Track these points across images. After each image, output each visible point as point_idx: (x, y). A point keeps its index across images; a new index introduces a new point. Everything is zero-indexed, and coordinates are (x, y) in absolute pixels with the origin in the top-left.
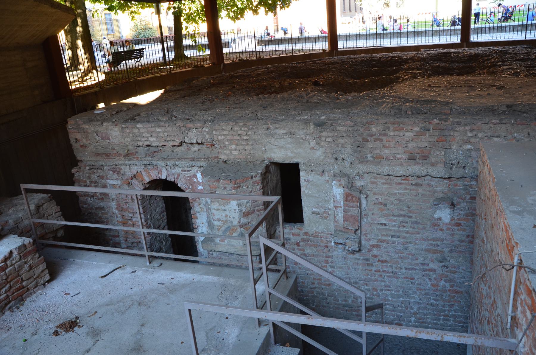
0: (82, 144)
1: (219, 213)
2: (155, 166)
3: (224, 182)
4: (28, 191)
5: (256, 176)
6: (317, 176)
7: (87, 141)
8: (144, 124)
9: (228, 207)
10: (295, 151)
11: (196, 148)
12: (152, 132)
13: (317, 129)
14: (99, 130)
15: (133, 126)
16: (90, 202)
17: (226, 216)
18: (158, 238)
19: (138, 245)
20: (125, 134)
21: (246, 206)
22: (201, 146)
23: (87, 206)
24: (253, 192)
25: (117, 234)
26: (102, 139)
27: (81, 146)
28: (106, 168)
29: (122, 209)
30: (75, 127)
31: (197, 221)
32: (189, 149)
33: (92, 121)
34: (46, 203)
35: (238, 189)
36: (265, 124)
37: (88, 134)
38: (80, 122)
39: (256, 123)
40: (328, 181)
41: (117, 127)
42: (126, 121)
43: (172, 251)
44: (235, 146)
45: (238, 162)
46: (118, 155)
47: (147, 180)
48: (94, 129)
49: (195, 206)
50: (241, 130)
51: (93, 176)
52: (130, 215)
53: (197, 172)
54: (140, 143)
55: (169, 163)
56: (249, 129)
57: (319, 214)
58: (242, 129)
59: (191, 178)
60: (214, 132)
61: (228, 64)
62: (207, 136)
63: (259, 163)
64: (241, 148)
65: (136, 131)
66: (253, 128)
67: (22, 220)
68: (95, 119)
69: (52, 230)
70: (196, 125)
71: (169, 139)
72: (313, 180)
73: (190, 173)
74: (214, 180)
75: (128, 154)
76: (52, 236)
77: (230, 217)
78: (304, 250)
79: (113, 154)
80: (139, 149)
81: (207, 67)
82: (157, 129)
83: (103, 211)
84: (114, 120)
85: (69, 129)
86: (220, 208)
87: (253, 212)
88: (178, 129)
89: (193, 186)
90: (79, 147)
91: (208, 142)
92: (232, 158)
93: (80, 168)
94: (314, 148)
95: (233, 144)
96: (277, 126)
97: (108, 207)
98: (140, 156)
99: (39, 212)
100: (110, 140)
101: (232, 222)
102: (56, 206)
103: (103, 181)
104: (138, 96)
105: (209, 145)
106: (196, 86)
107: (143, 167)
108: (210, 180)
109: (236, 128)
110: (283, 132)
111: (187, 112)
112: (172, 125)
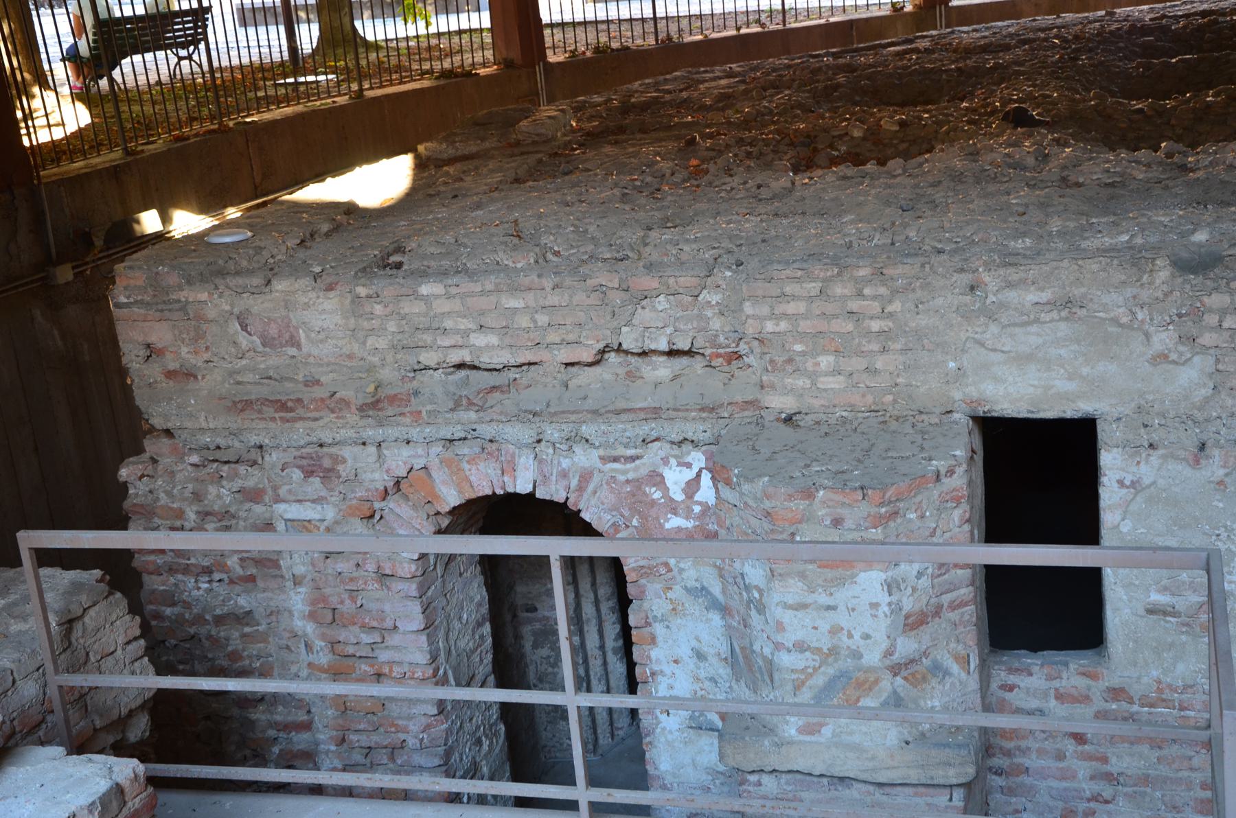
0: (173, 366)
1: (806, 618)
2: (487, 445)
3: (831, 495)
4: (46, 557)
5: (951, 472)
6: (1174, 466)
7: (196, 353)
8: (450, 282)
9: (842, 596)
10: (1085, 371)
11: (662, 369)
12: (482, 313)
13: (1189, 282)
14: (255, 310)
15: (404, 291)
16: (195, 593)
17: (835, 630)
18: (467, 726)
19: (392, 758)
20: (366, 324)
21: (914, 589)
22: (685, 360)
23: (177, 610)
24: (938, 532)
25: (302, 717)
26: (264, 345)
27: (170, 374)
28: (273, 458)
29: (335, 617)
30: (147, 298)
31: (654, 653)
32: (632, 376)
33: (222, 273)
34: (94, 605)
35: (892, 524)
36: (962, 270)
37: (204, 327)
38: (173, 279)
39: (923, 266)
40: (1221, 483)
41: (332, 294)
42: (365, 272)
43: (508, 774)
44: (831, 358)
45: (844, 421)
46: (333, 403)
47: (452, 498)
48: (232, 305)
49: (649, 594)
50: (860, 294)
51: (213, 490)
52: (366, 638)
53: (665, 461)
54: (428, 358)
55: (552, 432)
56: (895, 292)
57: (1175, 614)
58: (867, 291)
59: (639, 488)
60: (748, 308)
61: (559, 63)
62: (716, 324)
63: (935, 420)
64: (858, 363)
65: (414, 308)
66: (908, 288)
67: (14, 682)
68: (231, 266)
69: (115, 715)
70: (671, 281)
71: (553, 337)
72: (1154, 483)
73: (636, 469)
74: (791, 490)
75: (378, 401)
76: (111, 739)
77: (850, 636)
78: (1104, 760)
79: (314, 400)
80: (425, 379)
81: (487, 77)
82: (504, 301)
83: (247, 630)
84: (318, 269)
85: (117, 305)
86: (810, 599)
87: (937, 612)
88: (594, 299)
89: (644, 517)
90: (161, 377)
91: (720, 346)
92: (817, 403)
93: (154, 461)
94: (1166, 357)
95: (825, 351)
96: (1015, 277)
97: (274, 613)
98: (429, 407)
99: (70, 643)
100: (298, 346)
101: (857, 655)
102: (128, 617)
103: (258, 509)
104: (329, 180)
105: (718, 356)
106: (534, 143)
107: (437, 449)
108: (771, 490)
109: (839, 290)
110: (1036, 299)
111: (598, 234)
112: (568, 282)
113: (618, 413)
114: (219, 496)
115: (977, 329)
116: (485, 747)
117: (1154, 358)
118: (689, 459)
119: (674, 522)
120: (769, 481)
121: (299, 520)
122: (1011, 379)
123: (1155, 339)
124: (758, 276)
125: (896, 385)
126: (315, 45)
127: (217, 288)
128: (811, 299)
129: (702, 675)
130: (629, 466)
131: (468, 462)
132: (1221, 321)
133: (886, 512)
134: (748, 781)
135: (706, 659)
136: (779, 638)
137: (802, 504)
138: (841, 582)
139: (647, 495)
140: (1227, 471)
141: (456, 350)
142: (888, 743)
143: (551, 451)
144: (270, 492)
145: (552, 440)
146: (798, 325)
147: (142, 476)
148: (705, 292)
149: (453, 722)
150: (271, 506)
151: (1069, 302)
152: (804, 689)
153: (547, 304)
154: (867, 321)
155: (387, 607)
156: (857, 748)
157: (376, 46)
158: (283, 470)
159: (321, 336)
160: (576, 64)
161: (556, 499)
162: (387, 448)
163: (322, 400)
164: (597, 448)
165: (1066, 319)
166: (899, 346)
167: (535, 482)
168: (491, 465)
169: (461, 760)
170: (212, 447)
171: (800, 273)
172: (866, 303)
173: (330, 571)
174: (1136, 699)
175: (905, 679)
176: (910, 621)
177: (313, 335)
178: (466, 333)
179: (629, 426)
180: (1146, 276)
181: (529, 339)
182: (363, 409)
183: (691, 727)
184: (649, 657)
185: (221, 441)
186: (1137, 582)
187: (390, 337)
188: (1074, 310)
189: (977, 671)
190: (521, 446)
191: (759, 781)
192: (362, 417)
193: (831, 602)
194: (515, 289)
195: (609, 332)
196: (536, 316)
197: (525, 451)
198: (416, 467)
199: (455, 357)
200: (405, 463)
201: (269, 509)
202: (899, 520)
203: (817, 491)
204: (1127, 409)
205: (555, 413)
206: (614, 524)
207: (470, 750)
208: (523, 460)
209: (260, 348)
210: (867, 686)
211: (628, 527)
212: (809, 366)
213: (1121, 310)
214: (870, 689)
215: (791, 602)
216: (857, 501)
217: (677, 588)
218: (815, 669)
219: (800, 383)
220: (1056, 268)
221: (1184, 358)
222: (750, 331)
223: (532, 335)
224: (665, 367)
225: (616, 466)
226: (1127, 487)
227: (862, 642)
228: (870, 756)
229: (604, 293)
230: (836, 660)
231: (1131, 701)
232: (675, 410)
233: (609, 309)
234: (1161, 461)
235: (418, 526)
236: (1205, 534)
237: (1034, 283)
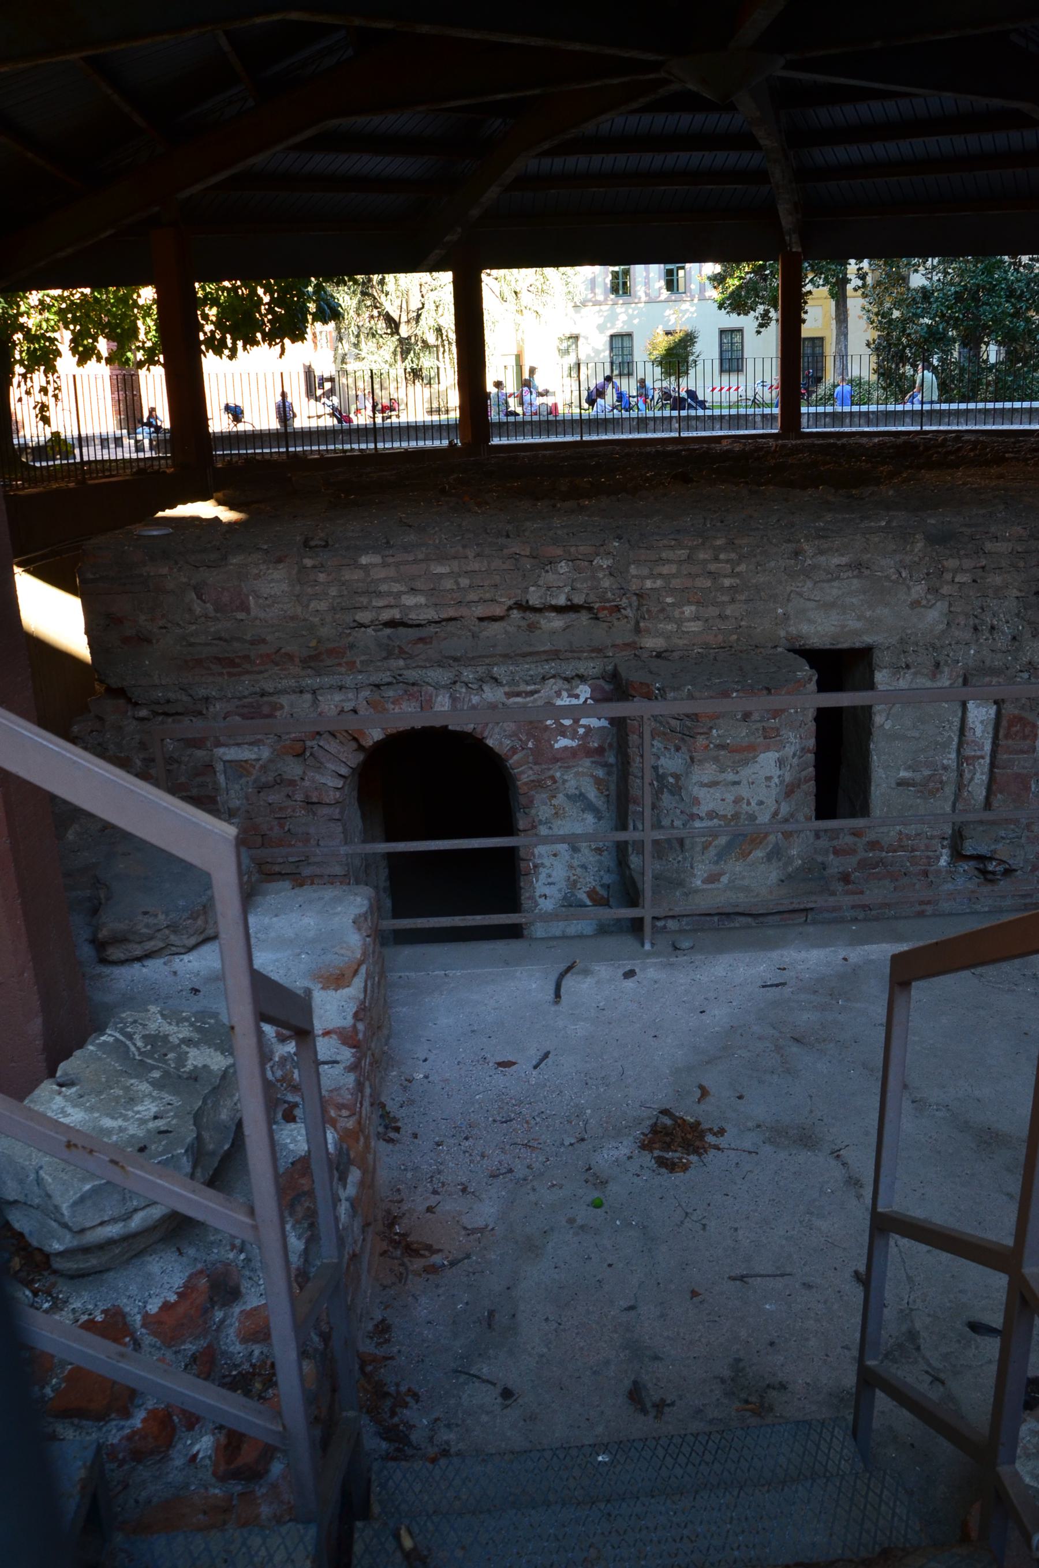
1: (717, 793)
8: (387, 553)
9: (746, 773)
11: (556, 622)
32: (532, 627)
36: (789, 541)
39: (762, 537)
41: (281, 566)
50: (716, 559)
54: (364, 617)
55: (468, 675)
56: (742, 558)
58: (722, 556)
60: (633, 570)
62: (606, 583)
64: (712, 611)
65: (358, 575)
70: (573, 549)
71: (473, 596)
73: (535, 700)
77: (749, 804)
86: (722, 777)
91: (609, 601)
92: (681, 642)
96: (826, 546)
98: (363, 658)
100: (246, 609)
101: (752, 817)
104: (189, 504)
107: (366, 693)
109: (701, 556)
113: (524, 655)
117: (912, 604)
118: (577, 691)
119: (563, 742)
121: (236, 761)
122: (820, 620)
125: (740, 627)
128: (680, 562)
129: (576, 863)
130: (528, 699)
131: (393, 703)
132: (953, 577)
134: (656, 926)
135: (579, 851)
136: (695, 810)
138: (746, 762)
141: (388, 610)
145: (466, 680)
146: (670, 583)
147: (92, 731)
150: (212, 750)
152: (711, 848)
153: (469, 569)
155: (312, 830)
165: (857, 577)
166: (744, 598)
168: (412, 705)
171: (673, 543)
172: (720, 565)
173: (262, 803)
177: (261, 601)
178: (398, 595)
179: (533, 666)
181: (452, 599)
183: (564, 906)
184: (533, 854)
185: (171, 695)
187: (331, 600)
190: (437, 687)
191: (665, 925)
192: (304, 668)
193: (736, 778)
194: (442, 558)
196: (460, 580)
197: (442, 691)
199: (386, 616)
200: (336, 706)
201: (209, 752)
204: (894, 640)
206: (512, 747)
208: (440, 698)
210: (758, 841)
211: (523, 749)
212: (677, 614)
213: (892, 570)
214: (761, 843)
215: (706, 781)
219: (669, 627)
225: (519, 700)
227: (757, 808)
231: (882, 849)
235: (344, 760)
236: (937, 727)
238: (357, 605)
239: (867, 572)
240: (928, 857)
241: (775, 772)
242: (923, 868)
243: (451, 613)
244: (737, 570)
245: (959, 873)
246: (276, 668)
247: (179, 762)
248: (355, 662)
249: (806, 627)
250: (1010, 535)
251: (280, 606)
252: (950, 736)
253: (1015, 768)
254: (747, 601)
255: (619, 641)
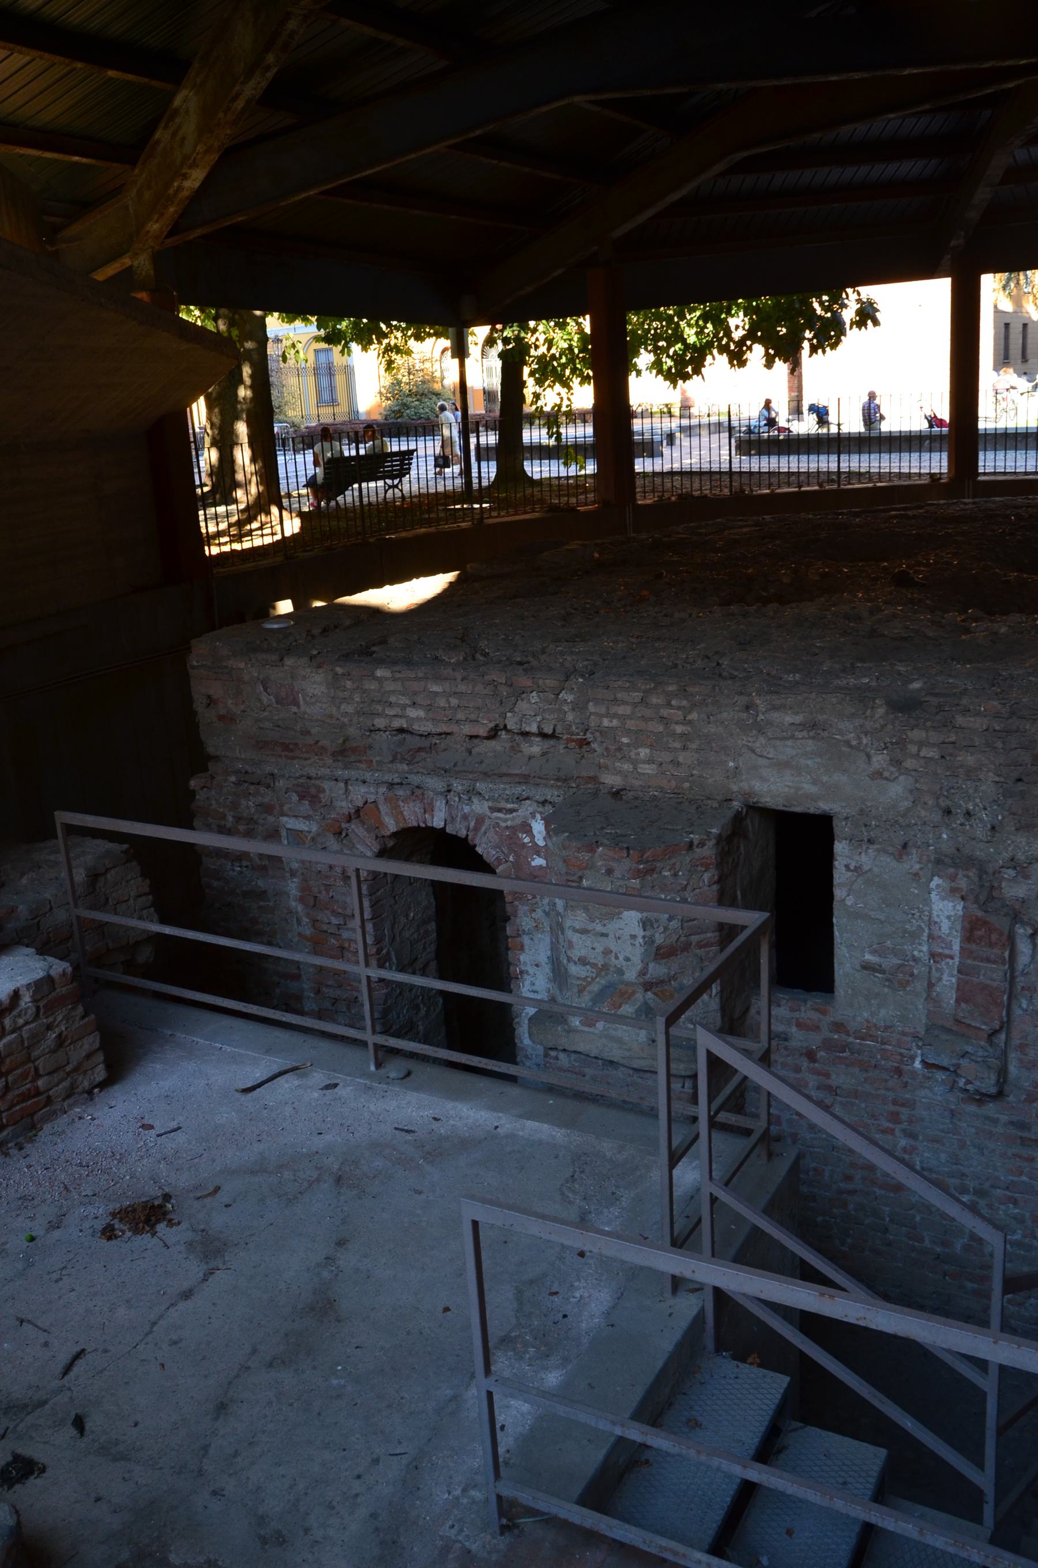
0: (222, 712)
4: (72, 830)
5: (702, 844)
6: (886, 859)
9: (612, 927)
10: (825, 779)
11: (535, 748)
12: (415, 693)
16: (231, 873)
17: (607, 952)
19: (349, 1008)
20: (341, 694)
21: (666, 929)
24: (689, 888)
26: (277, 703)
27: (221, 718)
28: (281, 784)
34: (115, 867)
36: (741, 694)
39: (714, 687)
40: (916, 874)
41: (321, 671)
42: (346, 657)
44: (648, 751)
45: (654, 798)
47: (391, 825)
49: (520, 913)
50: (669, 704)
52: (335, 921)
54: (380, 722)
55: (458, 786)
56: (694, 706)
57: (883, 972)
58: (673, 703)
59: (515, 834)
60: (591, 708)
63: (715, 805)
64: (665, 756)
65: (373, 686)
70: (541, 682)
71: (460, 716)
72: (870, 870)
73: (513, 819)
75: (344, 750)
77: (617, 958)
78: (827, 1075)
82: (429, 686)
83: (262, 903)
84: (315, 652)
85: (193, 667)
86: (590, 927)
89: (517, 856)
94: (881, 774)
95: (642, 746)
98: (378, 758)
100: (298, 705)
101: (620, 972)
102: (140, 879)
103: (271, 819)
104: (387, 587)
107: (383, 789)
109: (654, 700)
113: (501, 776)
114: (248, 807)
115: (750, 739)
116: (423, 1012)
119: (539, 862)
120: (568, 836)
122: (772, 779)
123: (874, 759)
124: (599, 684)
125: (692, 775)
126: (492, 480)
127: (250, 660)
130: (508, 816)
131: (403, 801)
132: (919, 751)
133: (643, 868)
134: (549, 1055)
137: (587, 856)
139: (520, 840)
140: (922, 866)
142: (640, 1040)
143: (457, 799)
144: (278, 808)
146: (626, 724)
148: (564, 692)
149: (392, 989)
151: (814, 726)
152: (585, 993)
153: (458, 690)
154: (673, 725)
156: (619, 1040)
157: (540, 482)
158: (286, 793)
159: (313, 700)
160: (662, 507)
161: (459, 835)
162: (351, 785)
163: (311, 745)
164: (487, 800)
165: (813, 738)
166: (694, 746)
167: (446, 821)
169: (398, 1017)
170: (243, 771)
171: (628, 684)
174: (851, 1032)
175: (655, 994)
176: (662, 951)
178: (404, 707)
180: (869, 711)
181: (445, 716)
182: (333, 754)
186: (856, 944)
188: (819, 731)
189: (718, 996)
193: (604, 931)
194: (438, 678)
195: (497, 716)
198: (370, 801)
199: (397, 724)
200: (362, 797)
202: (655, 876)
203: (598, 847)
205: (459, 772)
206: (497, 858)
207: (408, 1011)
208: (438, 803)
209: (275, 705)
210: (626, 996)
211: (506, 861)
212: (633, 755)
213: (852, 735)
214: (629, 998)
215: (578, 927)
216: (622, 857)
217: (539, 911)
218: (593, 979)
220: (807, 698)
221: (893, 777)
222: (592, 724)
223: (447, 712)
224: (538, 745)
226: (852, 871)
227: (624, 963)
228: (627, 1047)
229: (496, 686)
230: (607, 974)
231: (848, 1034)
232: (539, 778)
233: (499, 699)
234: (875, 853)
236: (904, 912)
237: (791, 708)
238: (375, 712)
239: (826, 734)
240: (901, 1054)
241: (640, 933)
242: (895, 1064)
243: (444, 728)
244: (689, 717)
245: (937, 1081)
246: (316, 758)
247: (256, 823)
248: (372, 761)
249: (758, 784)
250: (985, 710)
251: (320, 705)
252: (920, 926)
253: (981, 977)
254: (698, 750)
255: (584, 774)
